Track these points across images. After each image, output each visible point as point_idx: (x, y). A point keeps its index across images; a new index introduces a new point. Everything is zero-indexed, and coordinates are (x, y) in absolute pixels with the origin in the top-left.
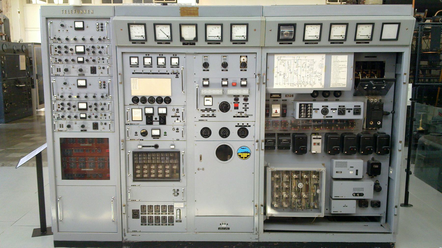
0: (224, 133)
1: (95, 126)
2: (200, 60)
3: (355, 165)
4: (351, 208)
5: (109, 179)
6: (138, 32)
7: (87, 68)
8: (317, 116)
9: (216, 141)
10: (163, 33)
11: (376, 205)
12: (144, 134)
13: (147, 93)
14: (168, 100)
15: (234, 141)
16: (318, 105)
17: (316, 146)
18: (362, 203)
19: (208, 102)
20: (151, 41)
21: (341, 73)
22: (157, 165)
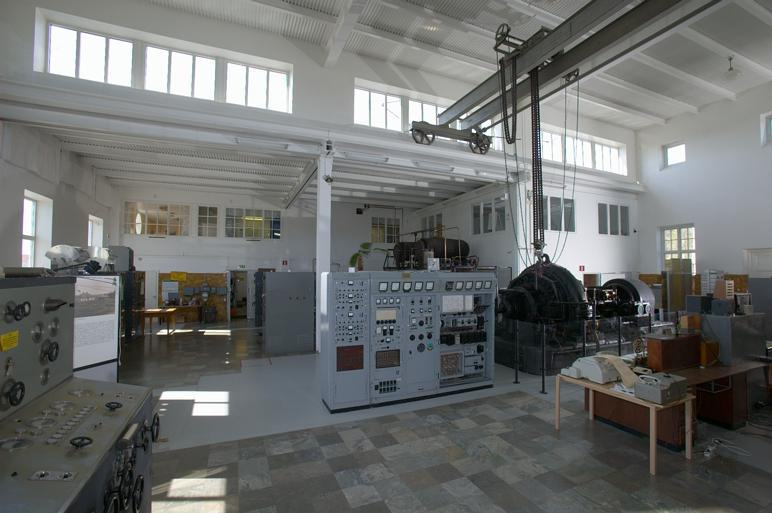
0: (421, 337)
1: (357, 339)
2: (409, 300)
3: (473, 347)
4: (472, 370)
5: (600, 233)
6: (383, 287)
7: (354, 305)
8: (459, 325)
9: (417, 341)
10: (395, 286)
11: (481, 367)
12: (382, 341)
13: (384, 319)
14: (394, 321)
15: (426, 341)
16: (460, 320)
17: (457, 339)
18: (476, 368)
19: (414, 321)
20: (389, 291)
21: (470, 306)
22: (389, 358)
